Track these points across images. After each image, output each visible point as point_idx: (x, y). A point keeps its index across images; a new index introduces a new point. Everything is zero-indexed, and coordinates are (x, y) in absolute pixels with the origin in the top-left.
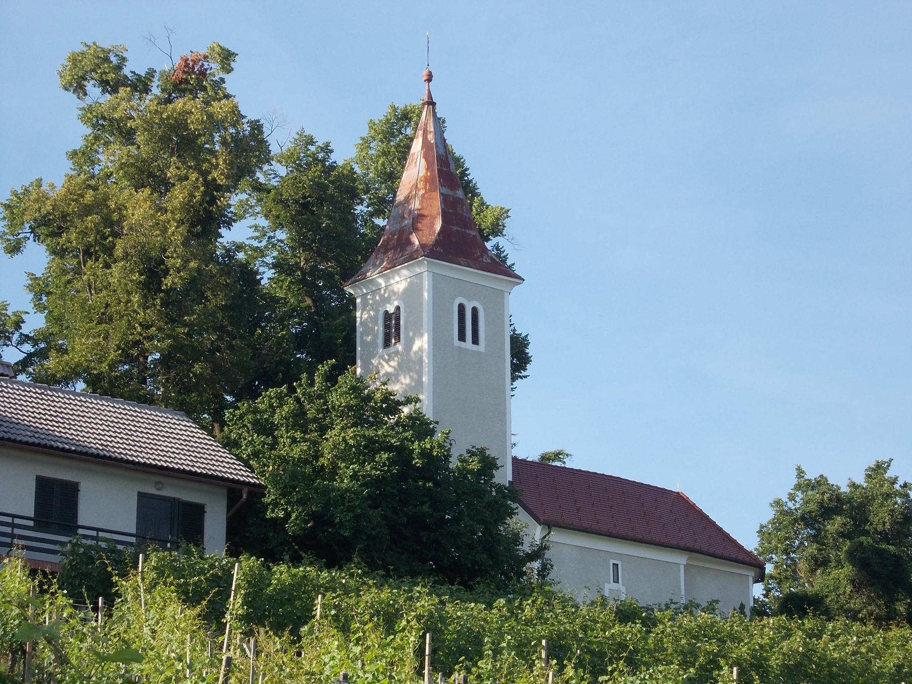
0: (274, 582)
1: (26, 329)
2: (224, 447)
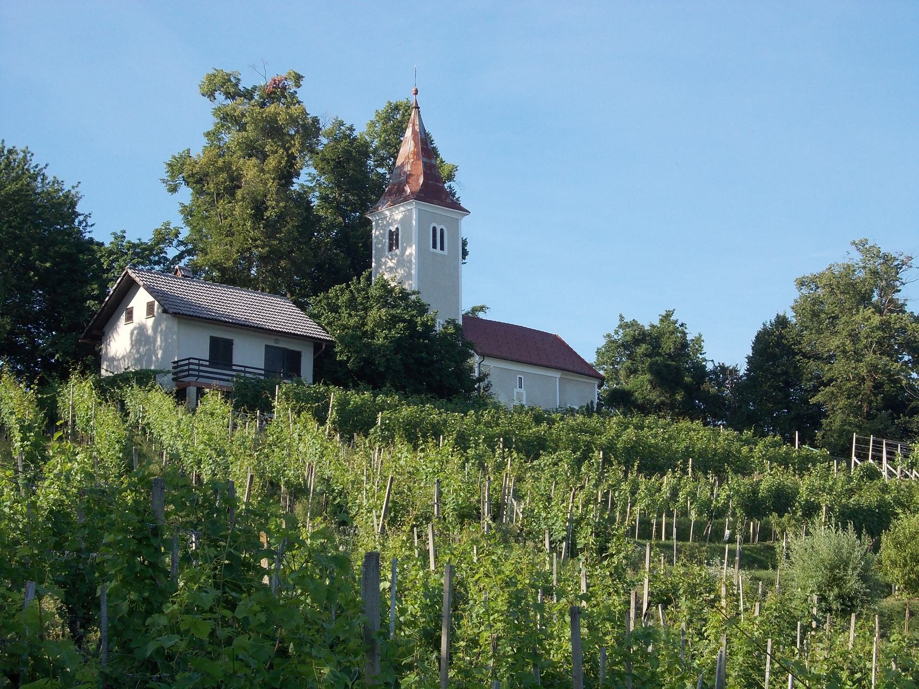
0: (352, 403)
1: (181, 238)
2: (293, 304)
